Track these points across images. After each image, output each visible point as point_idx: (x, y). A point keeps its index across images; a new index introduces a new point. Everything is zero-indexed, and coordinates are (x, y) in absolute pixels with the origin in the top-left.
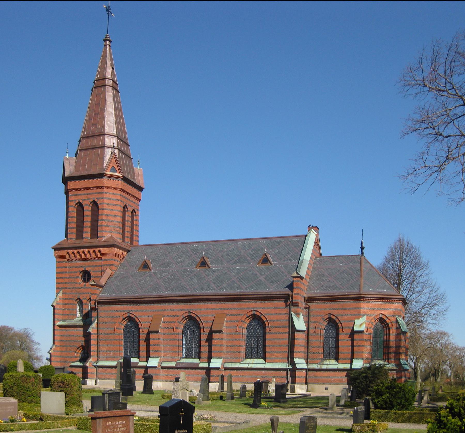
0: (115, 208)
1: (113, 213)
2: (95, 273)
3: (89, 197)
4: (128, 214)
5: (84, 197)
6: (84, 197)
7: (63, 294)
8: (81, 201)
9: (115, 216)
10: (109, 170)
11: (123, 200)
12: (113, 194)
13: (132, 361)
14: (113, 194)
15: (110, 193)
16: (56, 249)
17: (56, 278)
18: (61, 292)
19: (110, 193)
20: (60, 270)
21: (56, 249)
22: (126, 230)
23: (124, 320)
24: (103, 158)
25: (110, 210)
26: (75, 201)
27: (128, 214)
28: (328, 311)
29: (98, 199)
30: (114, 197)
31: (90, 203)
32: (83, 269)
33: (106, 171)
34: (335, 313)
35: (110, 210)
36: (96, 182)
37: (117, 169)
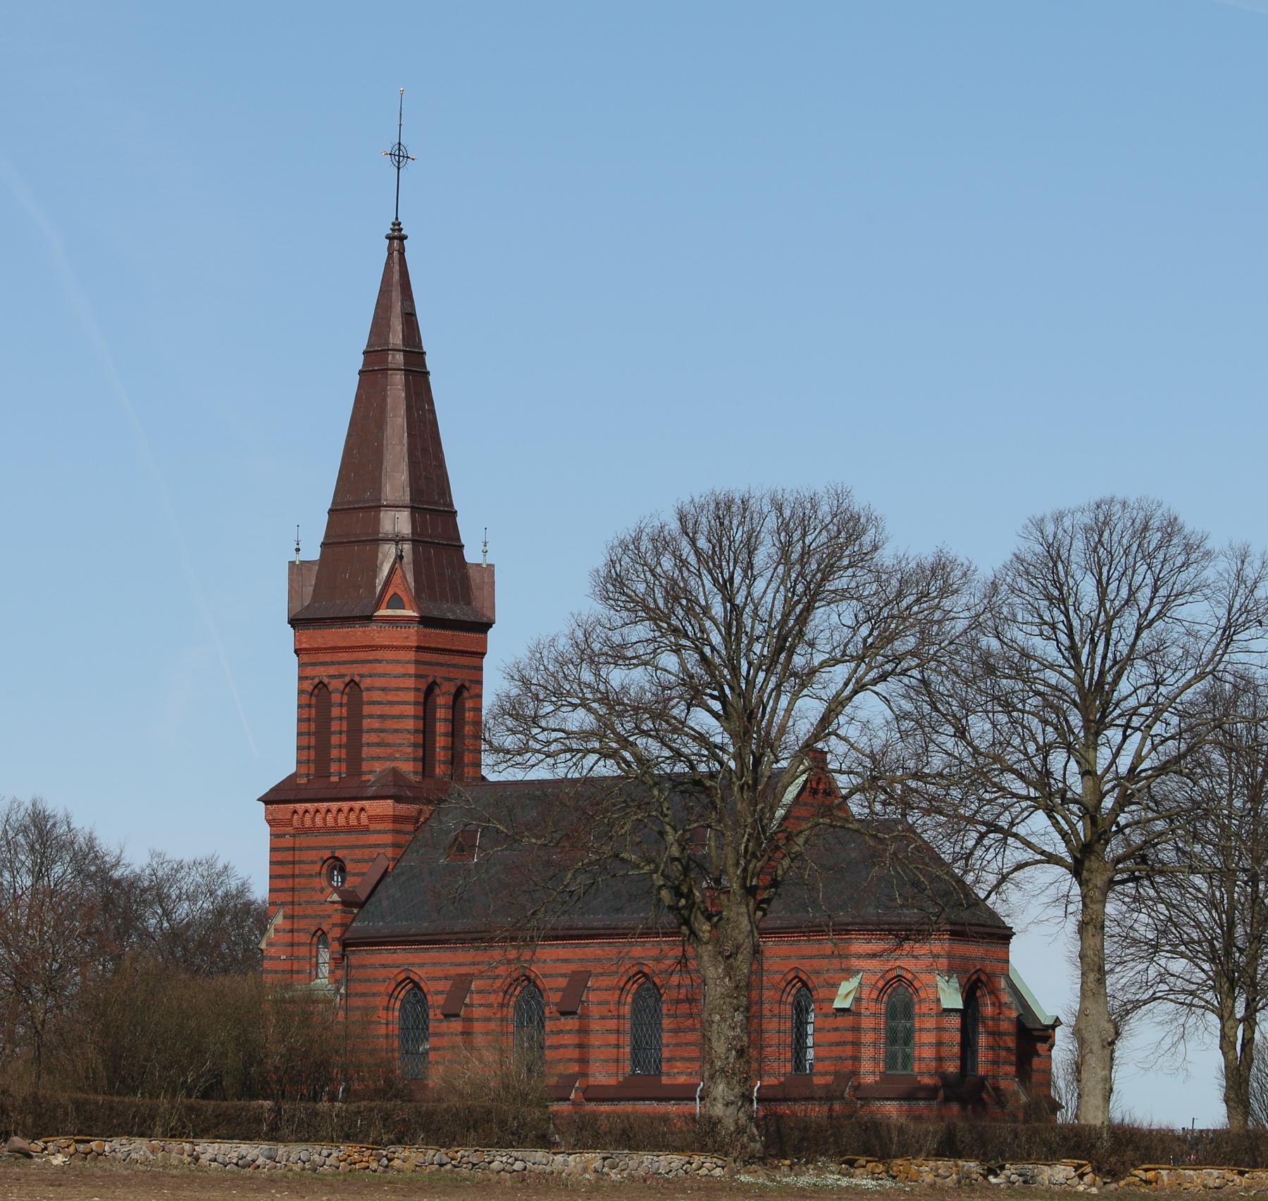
0: (402, 696)
1: (396, 710)
2: (354, 865)
3: (343, 669)
4: (442, 701)
5: (332, 670)
6: (332, 670)
7: (285, 917)
8: (326, 681)
9: (401, 717)
10: (384, 604)
11: (423, 673)
12: (398, 662)
13: (815, 1082)
14: (398, 662)
15: (388, 662)
16: (267, 800)
17: (271, 877)
18: (281, 913)
19: (388, 662)
20: (463, 640)
21: (267, 800)
22: (438, 745)
23: (399, 989)
24: (374, 569)
25: (391, 703)
26: (313, 679)
27: (442, 701)
28: (794, 963)
29: (361, 676)
30: (399, 670)
31: (343, 686)
32: (328, 854)
33: (377, 607)
34: (806, 965)
35: (391, 703)
36: (357, 634)
37: (405, 599)
